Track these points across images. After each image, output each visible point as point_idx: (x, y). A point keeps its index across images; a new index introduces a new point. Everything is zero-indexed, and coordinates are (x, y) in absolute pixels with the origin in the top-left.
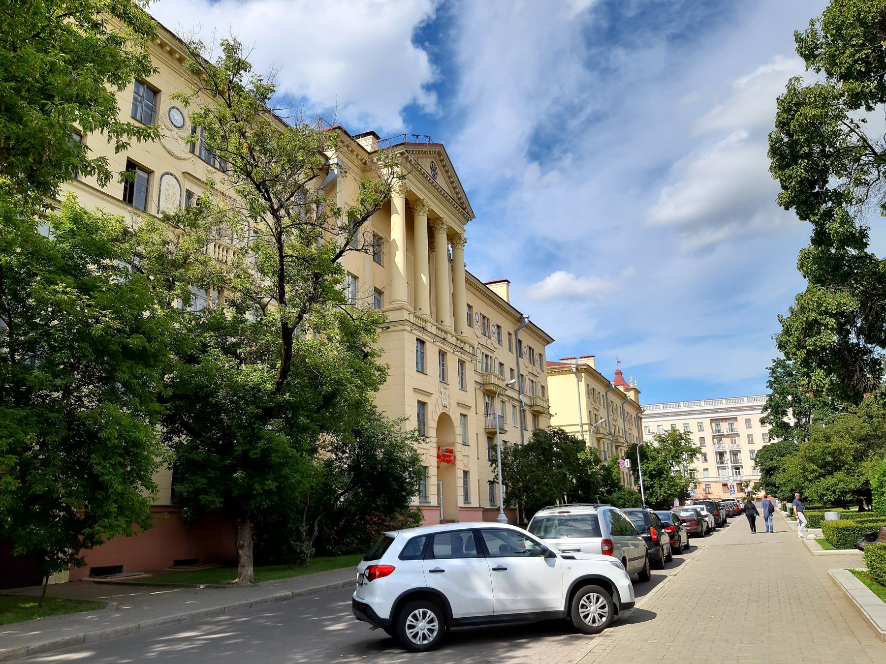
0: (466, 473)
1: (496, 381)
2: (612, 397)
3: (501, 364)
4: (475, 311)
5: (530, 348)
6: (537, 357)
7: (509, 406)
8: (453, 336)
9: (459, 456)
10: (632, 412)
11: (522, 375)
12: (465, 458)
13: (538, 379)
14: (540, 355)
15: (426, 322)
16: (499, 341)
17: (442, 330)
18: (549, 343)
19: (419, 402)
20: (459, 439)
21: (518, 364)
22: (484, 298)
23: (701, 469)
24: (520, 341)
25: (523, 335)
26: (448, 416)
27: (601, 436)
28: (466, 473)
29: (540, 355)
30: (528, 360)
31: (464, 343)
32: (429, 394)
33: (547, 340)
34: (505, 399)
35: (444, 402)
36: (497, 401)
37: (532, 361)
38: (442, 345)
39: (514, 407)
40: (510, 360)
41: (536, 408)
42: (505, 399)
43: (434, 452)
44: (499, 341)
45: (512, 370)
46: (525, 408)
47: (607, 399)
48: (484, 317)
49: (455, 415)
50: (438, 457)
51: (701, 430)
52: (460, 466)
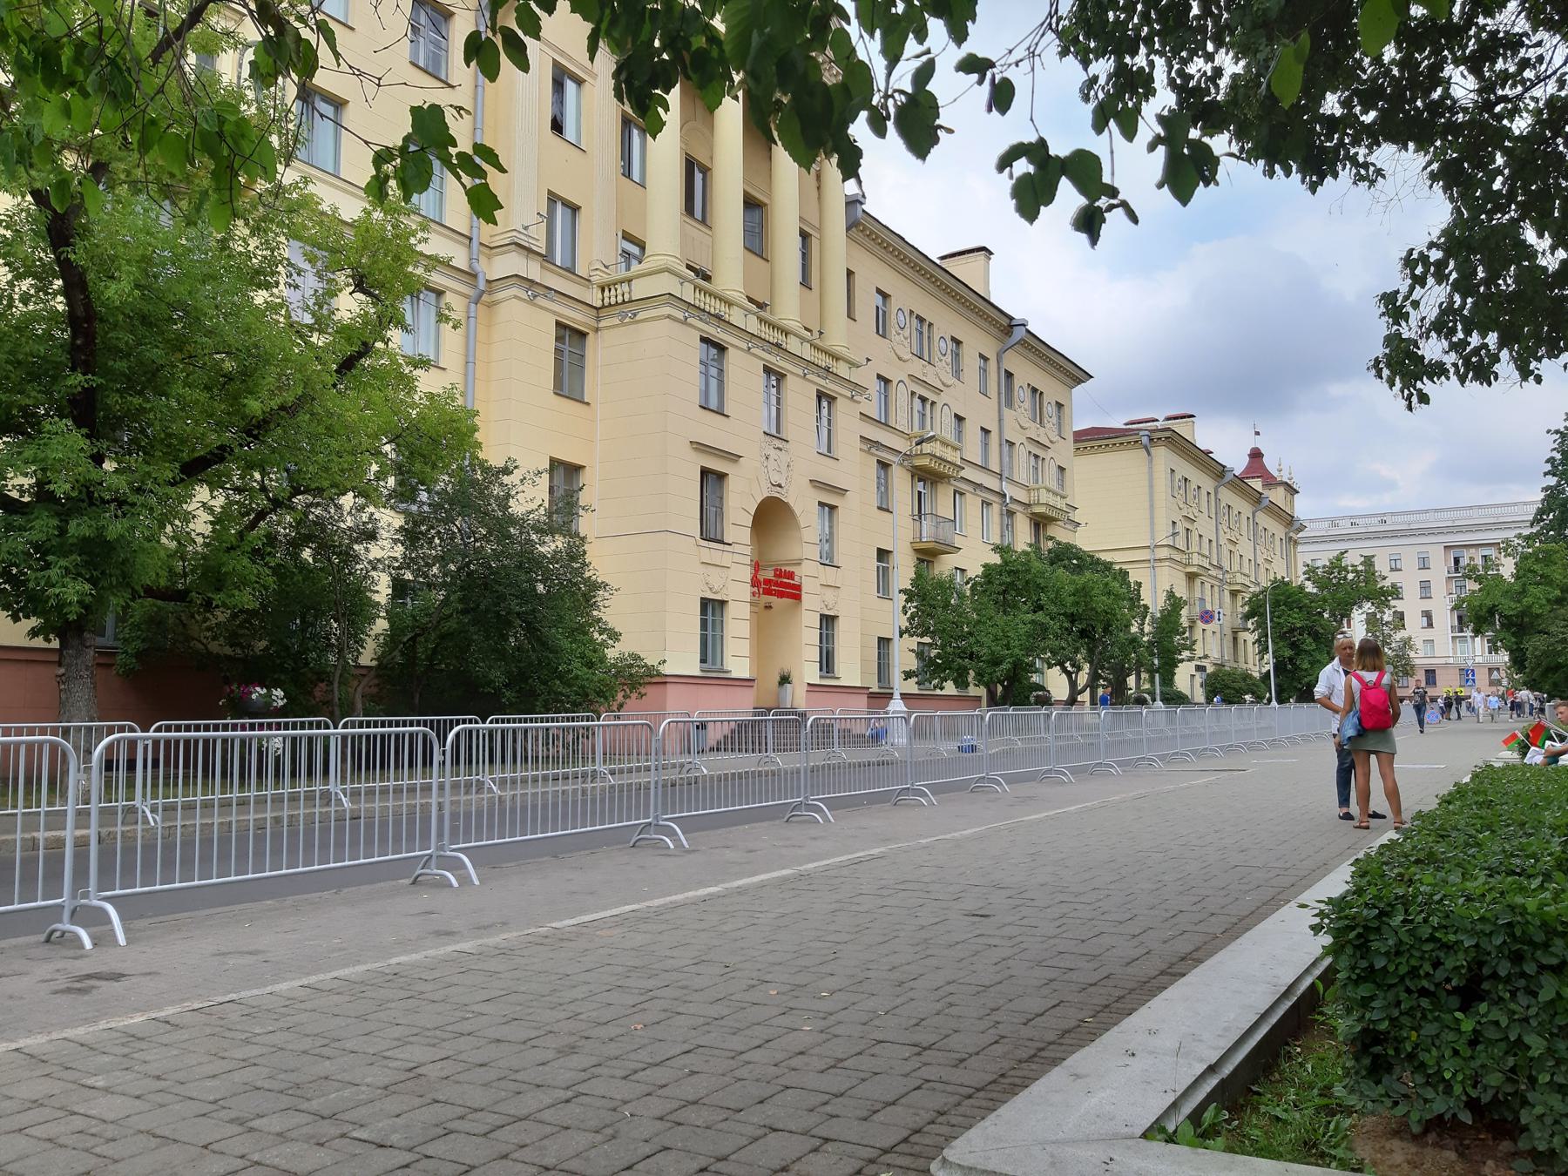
0: (828, 621)
1: (1052, 500)
2: (1264, 520)
3: (959, 419)
4: (894, 304)
5: (1034, 390)
6: (1050, 410)
7: (972, 503)
8: (803, 340)
9: (808, 587)
10: (1278, 530)
11: (1011, 444)
12: (829, 593)
13: (1050, 453)
14: (1059, 405)
15: (730, 304)
16: (957, 373)
17: (773, 326)
18: (1080, 381)
19: (705, 472)
20: (812, 552)
21: (1000, 420)
22: (921, 280)
23: (1418, 642)
24: (1009, 375)
25: (1014, 362)
26: (786, 504)
27: (1194, 569)
28: (828, 621)
29: (1059, 405)
30: (1029, 414)
31: (837, 358)
32: (842, 492)
33: (1075, 375)
34: (963, 486)
35: (776, 479)
36: (1198, 582)
37: (1038, 416)
38: (822, 382)
39: (986, 504)
40: (981, 412)
41: (1037, 510)
42: (963, 486)
43: (746, 574)
44: (957, 373)
45: (986, 431)
46: (1014, 507)
47: (1218, 500)
48: (921, 320)
49: (804, 504)
50: (755, 582)
51: (1424, 566)
52: (812, 605)
